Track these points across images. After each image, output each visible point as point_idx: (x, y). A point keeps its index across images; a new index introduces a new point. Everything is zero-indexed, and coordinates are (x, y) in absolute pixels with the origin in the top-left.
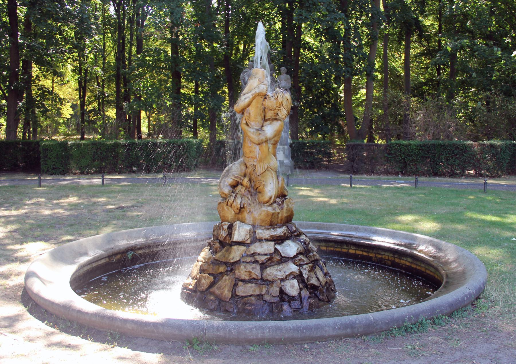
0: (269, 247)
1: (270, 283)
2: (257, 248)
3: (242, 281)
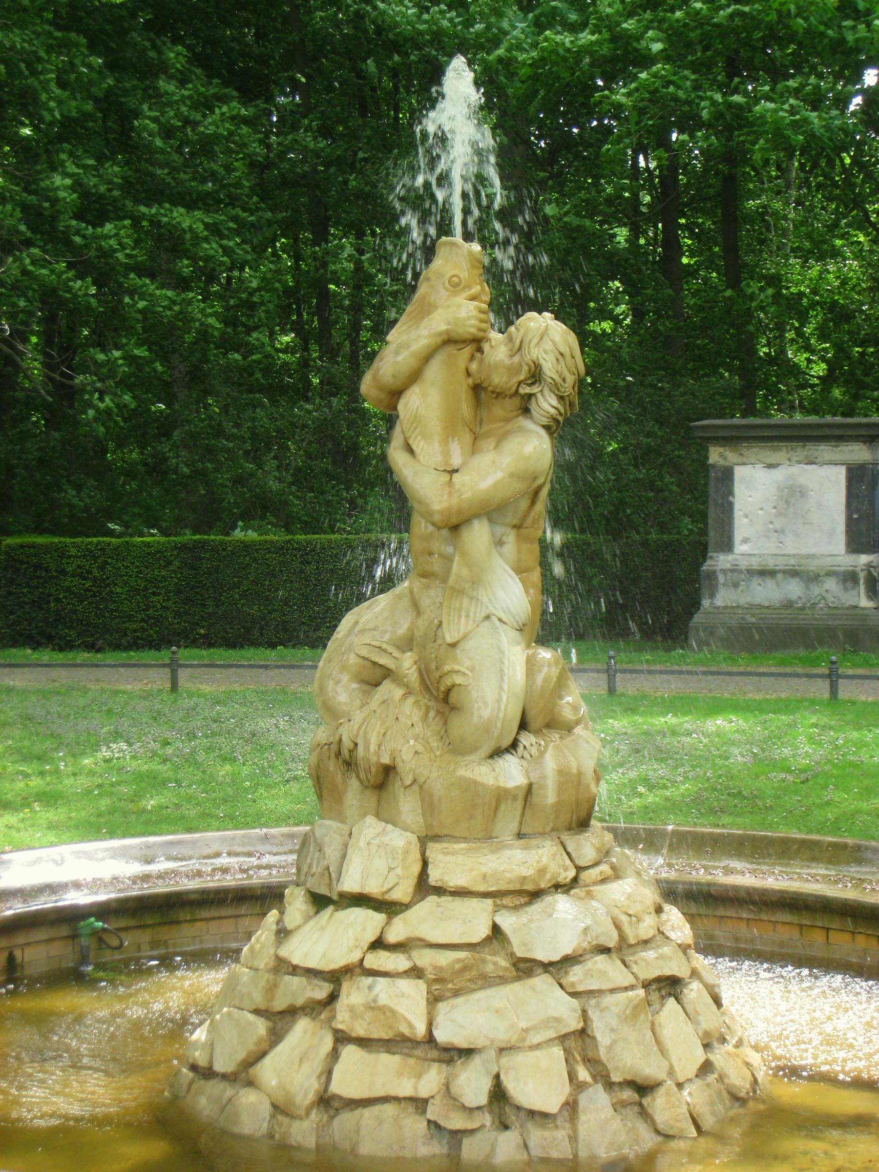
0: (471, 921)
1: (455, 1055)
2: (425, 920)
3: (364, 1043)
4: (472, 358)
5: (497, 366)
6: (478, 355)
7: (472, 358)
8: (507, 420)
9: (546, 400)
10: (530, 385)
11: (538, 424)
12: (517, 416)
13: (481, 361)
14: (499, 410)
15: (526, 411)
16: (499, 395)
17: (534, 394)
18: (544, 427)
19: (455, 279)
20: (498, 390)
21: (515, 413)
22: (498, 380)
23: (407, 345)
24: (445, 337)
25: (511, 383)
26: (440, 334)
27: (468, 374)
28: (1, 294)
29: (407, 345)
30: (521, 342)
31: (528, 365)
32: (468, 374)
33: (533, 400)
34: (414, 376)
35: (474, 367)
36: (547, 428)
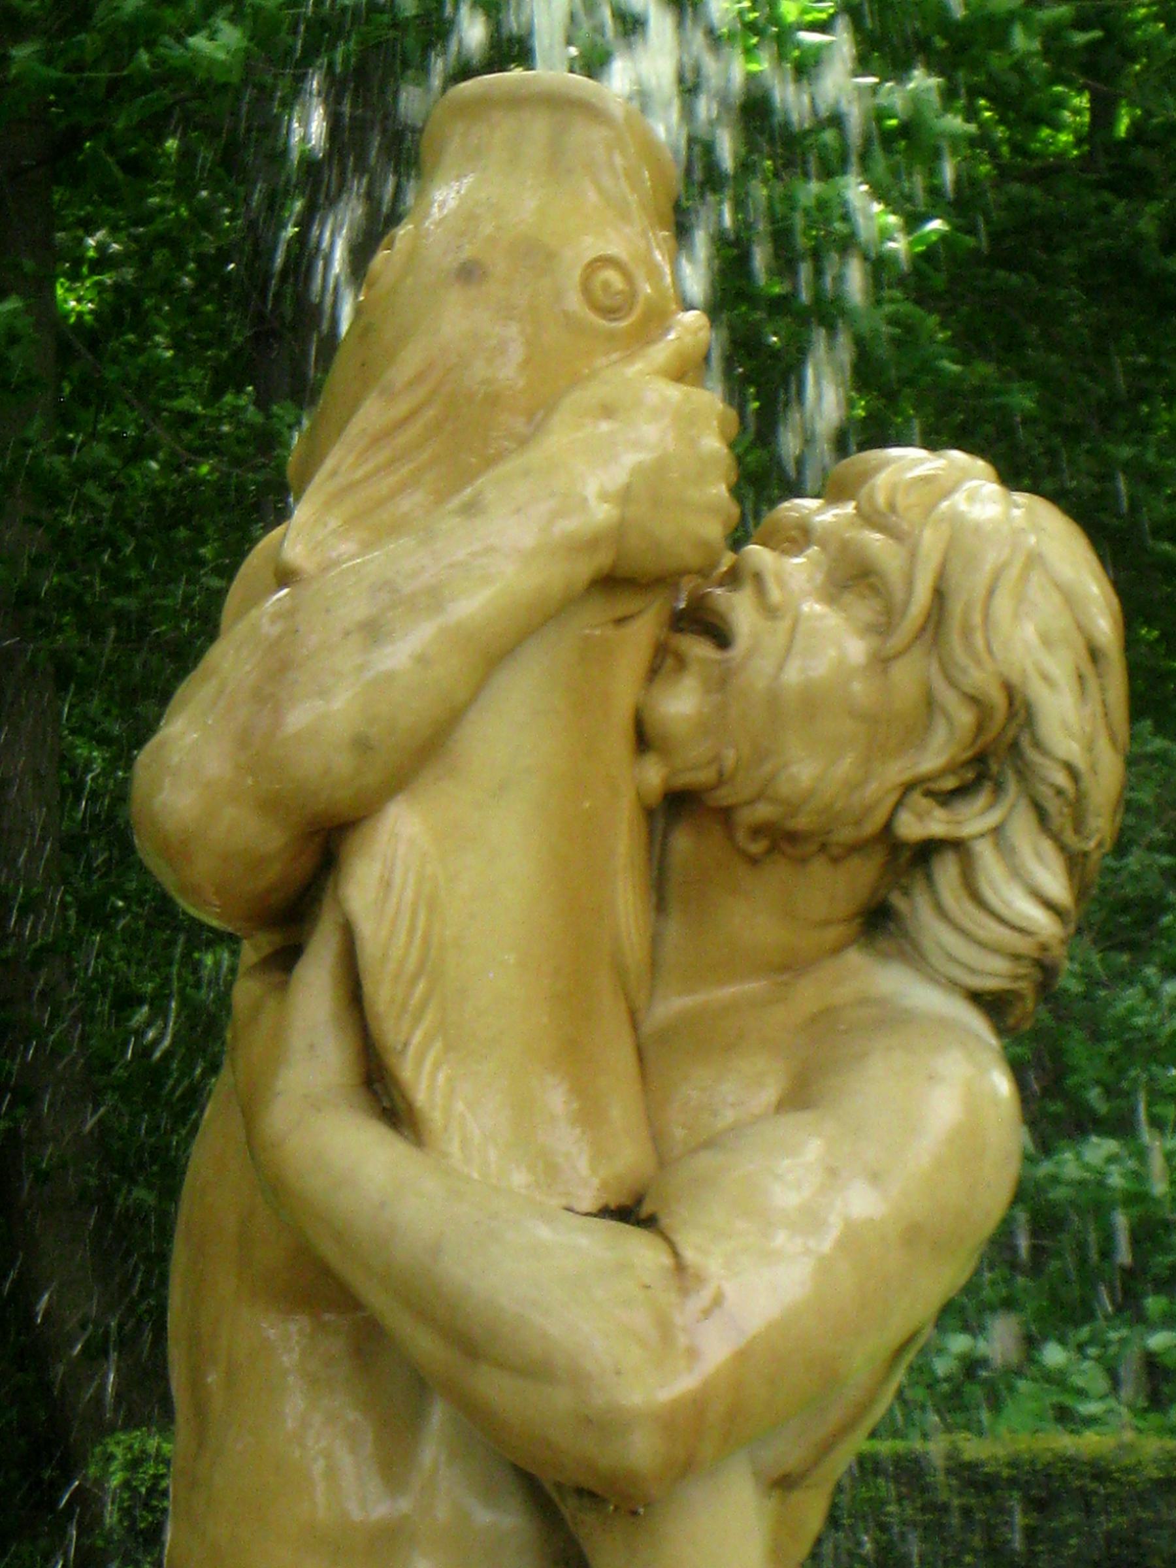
4: (662, 663)
5: (812, 703)
6: (699, 649)
7: (662, 663)
8: (790, 967)
9: (1017, 873)
10: (946, 799)
11: (953, 985)
12: (837, 950)
13: (721, 682)
14: (754, 915)
15: (877, 922)
16: (784, 841)
17: (958, 845)
18: (976, 998)
19: (612, 276)
20: (802, 822)
21: (833, 934)
22: (812, 772)
23: (434, 599)
24: (602, 560)
25: (872, 789)
26: (592, 544)
27: (644, 739)
28: (63, 1566)
29: (434, 599)
30: (939, 595)
31: (974, 700)
32: (644, 739)
33: (947, 871)
34: (419, 753)
35: (681, 703)
36: (993, 1005)
